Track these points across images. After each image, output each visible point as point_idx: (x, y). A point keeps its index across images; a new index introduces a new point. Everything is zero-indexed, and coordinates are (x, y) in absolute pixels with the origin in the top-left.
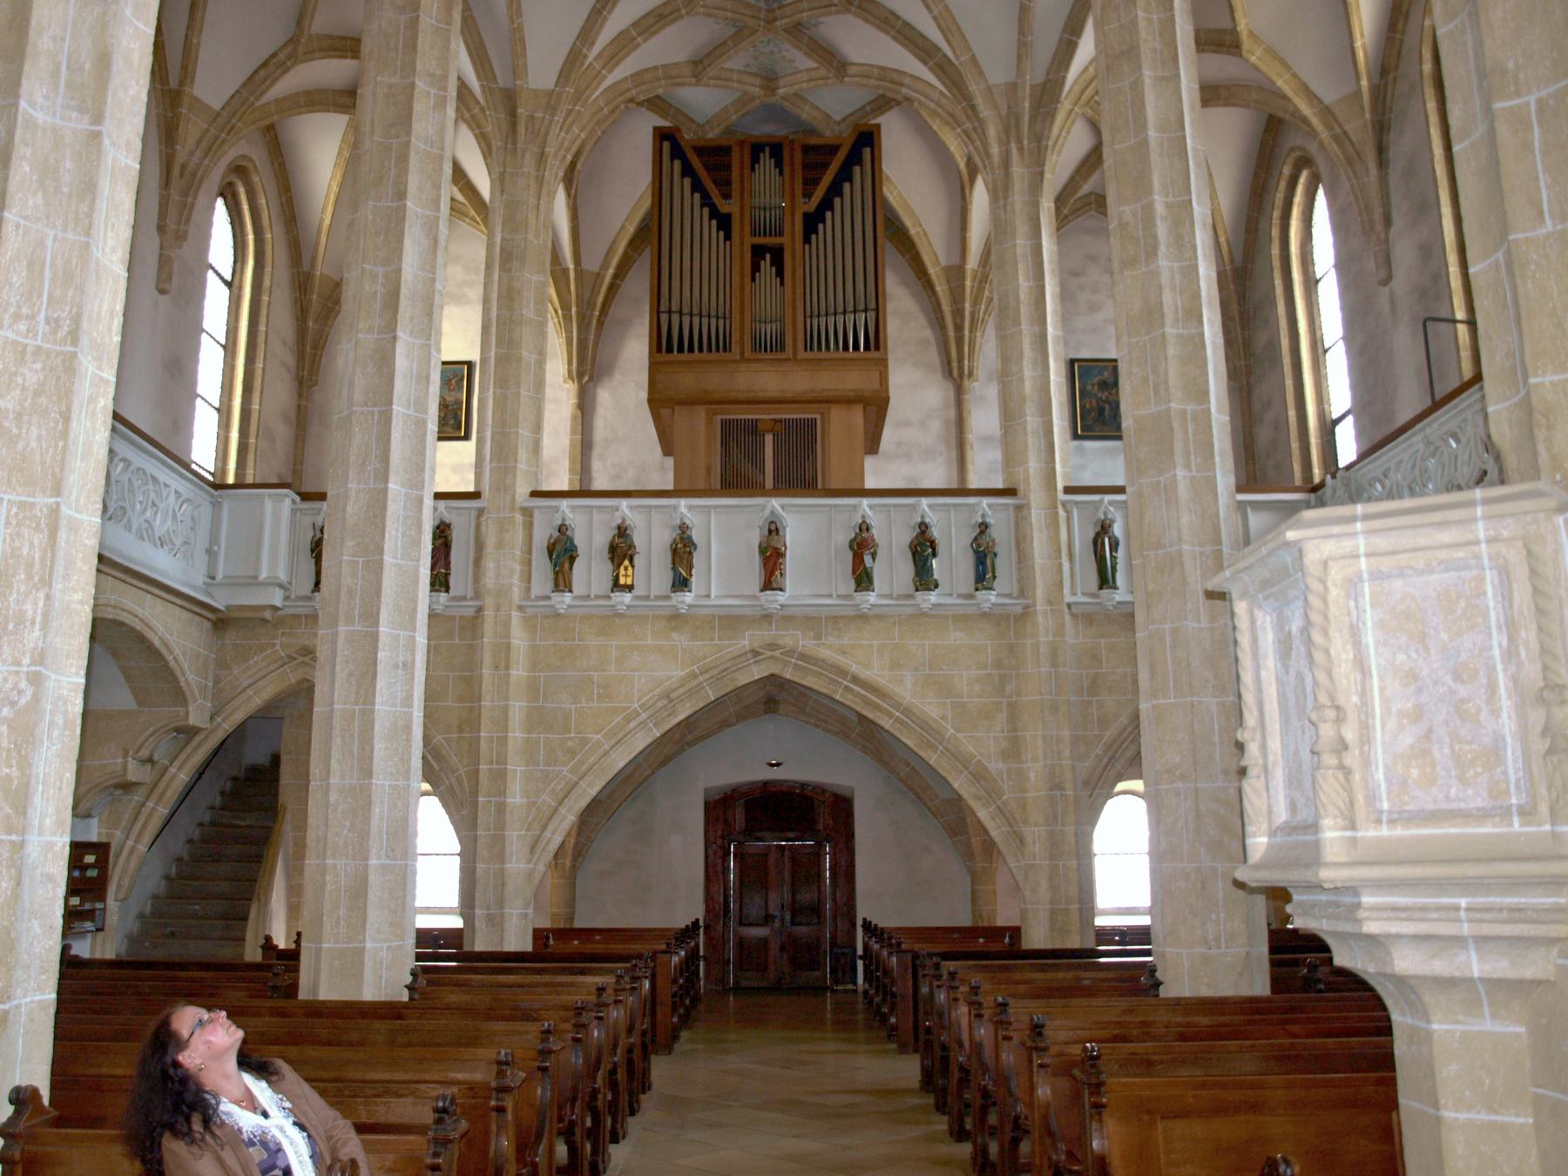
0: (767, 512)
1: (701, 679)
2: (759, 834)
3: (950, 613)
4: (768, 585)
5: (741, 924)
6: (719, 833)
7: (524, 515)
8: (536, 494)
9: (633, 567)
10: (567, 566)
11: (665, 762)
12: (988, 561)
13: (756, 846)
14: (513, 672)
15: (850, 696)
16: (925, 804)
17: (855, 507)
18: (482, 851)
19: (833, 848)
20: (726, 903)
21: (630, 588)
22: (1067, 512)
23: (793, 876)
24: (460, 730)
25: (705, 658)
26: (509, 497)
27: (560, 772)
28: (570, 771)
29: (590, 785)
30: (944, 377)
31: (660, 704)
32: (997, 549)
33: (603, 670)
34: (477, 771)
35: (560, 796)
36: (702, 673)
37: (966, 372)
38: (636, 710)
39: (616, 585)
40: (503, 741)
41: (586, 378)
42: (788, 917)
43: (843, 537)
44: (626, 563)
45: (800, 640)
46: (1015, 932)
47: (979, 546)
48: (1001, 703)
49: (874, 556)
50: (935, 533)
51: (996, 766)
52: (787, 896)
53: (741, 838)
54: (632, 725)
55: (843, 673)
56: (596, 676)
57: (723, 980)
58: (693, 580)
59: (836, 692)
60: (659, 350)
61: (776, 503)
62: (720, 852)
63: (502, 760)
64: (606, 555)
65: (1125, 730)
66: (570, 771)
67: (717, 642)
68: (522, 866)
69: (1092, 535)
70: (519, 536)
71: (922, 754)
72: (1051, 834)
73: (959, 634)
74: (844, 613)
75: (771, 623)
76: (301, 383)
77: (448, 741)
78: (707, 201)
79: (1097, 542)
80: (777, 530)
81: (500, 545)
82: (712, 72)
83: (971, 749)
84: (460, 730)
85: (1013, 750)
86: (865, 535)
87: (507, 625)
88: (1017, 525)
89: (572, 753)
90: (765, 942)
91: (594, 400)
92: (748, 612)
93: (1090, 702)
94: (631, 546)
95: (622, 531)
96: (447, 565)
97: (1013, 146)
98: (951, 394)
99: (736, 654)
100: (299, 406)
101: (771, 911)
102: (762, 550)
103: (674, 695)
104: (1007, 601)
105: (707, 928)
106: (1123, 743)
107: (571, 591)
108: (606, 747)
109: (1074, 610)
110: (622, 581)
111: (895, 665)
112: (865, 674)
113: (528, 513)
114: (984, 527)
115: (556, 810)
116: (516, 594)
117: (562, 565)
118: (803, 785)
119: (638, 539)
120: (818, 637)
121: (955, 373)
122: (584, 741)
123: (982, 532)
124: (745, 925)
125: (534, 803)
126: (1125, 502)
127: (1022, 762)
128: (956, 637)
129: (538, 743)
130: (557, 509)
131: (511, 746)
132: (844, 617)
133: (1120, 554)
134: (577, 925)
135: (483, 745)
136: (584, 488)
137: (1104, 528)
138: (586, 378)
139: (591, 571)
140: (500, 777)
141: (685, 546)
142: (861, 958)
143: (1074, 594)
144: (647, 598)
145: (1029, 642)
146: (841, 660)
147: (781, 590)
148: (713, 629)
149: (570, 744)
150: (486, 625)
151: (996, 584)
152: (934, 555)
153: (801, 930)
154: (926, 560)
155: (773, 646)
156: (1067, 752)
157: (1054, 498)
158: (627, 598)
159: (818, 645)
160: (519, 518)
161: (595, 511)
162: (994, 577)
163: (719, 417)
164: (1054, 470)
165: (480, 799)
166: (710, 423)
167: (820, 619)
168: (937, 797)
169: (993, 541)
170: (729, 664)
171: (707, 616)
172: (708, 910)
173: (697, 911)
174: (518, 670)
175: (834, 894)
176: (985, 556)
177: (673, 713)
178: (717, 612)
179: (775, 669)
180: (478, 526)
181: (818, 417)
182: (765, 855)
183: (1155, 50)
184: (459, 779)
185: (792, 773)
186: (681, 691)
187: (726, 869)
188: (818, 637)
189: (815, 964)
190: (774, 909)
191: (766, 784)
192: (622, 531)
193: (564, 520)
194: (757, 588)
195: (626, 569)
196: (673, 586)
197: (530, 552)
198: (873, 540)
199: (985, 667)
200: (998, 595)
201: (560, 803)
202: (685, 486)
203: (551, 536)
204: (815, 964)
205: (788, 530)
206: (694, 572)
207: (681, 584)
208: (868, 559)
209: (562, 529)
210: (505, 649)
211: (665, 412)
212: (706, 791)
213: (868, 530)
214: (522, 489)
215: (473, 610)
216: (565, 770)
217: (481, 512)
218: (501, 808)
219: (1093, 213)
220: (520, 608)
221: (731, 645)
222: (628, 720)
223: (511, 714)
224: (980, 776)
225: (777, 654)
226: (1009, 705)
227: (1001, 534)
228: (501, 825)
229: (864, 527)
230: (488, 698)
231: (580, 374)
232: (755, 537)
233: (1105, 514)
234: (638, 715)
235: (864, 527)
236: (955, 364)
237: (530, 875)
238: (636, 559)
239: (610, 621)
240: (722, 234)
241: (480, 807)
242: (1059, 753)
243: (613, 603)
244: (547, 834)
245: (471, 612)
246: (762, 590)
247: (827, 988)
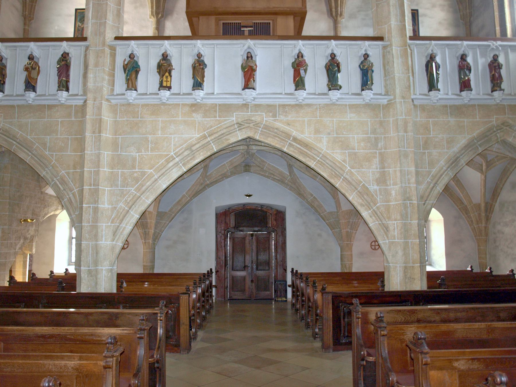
0: (246, 47)
1: (209, 139)
2: (241, 229)
3: (348, 103)
4: (247, 86)
5: (233, 270)
6: (223, 228)
7: (111, 49)
8: (117, 38)
9: (171, 76)
10: (134, 76)
11: (197, 194)
12: (369, 75)
13: (240, 234)
14: (103, 135)
15: (292, 149)
16: (319, 214)
18: (85, 234)
19: (276, 235)
20: (226, 260)
21: (169, 88)
22: (411, 50)
23: (257, 248)
24: (75, 168)
25: (211, 127)
26: (102, 38)
27: (131, 190)
28: (135, 190)
29: (147, 198)
30: (328, 17)
31: (186, 153)
32: (374, 69)
33: (154, 134)
34: (83, 190)
35: (130, 204)
36: (209, 136)
37: (339, 13)
38: (172, 156)
39: (162, 86)
40: (97, 173)
41: (160, 15)
42: (255, 267)
43: (288, 62)
44: (167, 74)
45: (266, 118)
46: (379, 276)
47: (364, 66)
48: (376, 153)
49: (305, 71)
50: (339, 59)
51: (373, 188)
52: (255, 258)
53: (233, 230)
54: (171, 164)
55: (288, 135)
57: (225, 296)
58: (205, 84)
59: (285, 147)
61: (250, 43)
62: (223, 237)
63: (97, 184)
65: (442, 168)
66: (135, 190)
67: (218, 118)
68: (108, 243)
69: (424, 63)
70: (108, 60)
71: (332, 181)
72: (405, 225)
73: (353, 115)
74: (289, 103)
75: (248, 108)
76: (25, 18)
77: (68, 173)
79: (428, 66)
80: (252, 57)
81: (96, 65)
83: (360, 178)
84: (75, 168)
85: (382, 179)
86: (300, 59)
87: (100, 108)
88: (384, 56)
89: (137, 180)
90: (244, 278)
91: (164, 27)
94: (170, 65)
95: (165, 57)
96: (68, 76)
98: (332, 24)
99: (228, 125)
100: (24, 29)
101: (246, 264)
102: (243, 68)
103: (194, 148)
105: (217, 272)
106: (441, 176)
107: (136, 90)
108: (156, 177)
110: (165, 84)
111: (317, 131)
112: (300, 136)
113: (113, 49)
114: (366, 56)
116: (106, 91)
117: (131, 76)
118: (262, 206)
119: (174, 63)
120: (274, 116)
121: (334, 14)
122: (144, 173)
123: (365, 59)
124: (235, 270)
125: (115, 208)
127: (387, 185)
128: (351, 116)
129: (118, 174)
131: (101, 175)
132: (289, 105)
133: (440, 72)
134: (156, 271)
135: (86, 174)
137: (432, 58)
138: (160, 15)
140: (95, 193)
141: (200, 65)
142: (289, 286)
145: (391, 119)
146: (287, 128)
147: (254, 89)
148: (215, 111)
149: (135, 175)
150: (88, 109)
151: (373, 87)
152: (339, 71)
153: (260, 273)
154: (335, 74)
155: (249, 121)
156: (413, 180)
157: (406, 42)
158: (167, 93)
159: (275, 120)
160: (107, 50)
162: (372, 84)
163: (222, 22)
164: (405, 26)
165: (84, 205)
166: (217, 24)
168: (326, 211)
169: (372, 64)
170: (225, 131)
171: (213, 104)
172: (218, 263)
173: (212, 265)
174: (106, 134)
175: (276, 256)
176: (367, 72)
177: (193, 158)
179: (250, 134)
180: (86, 56)
181: (271, 22)
182: (244, 239)
184: (74, 195)
185: (256, 200)
186: (197, 146)
187: (225, 246)
188: (274, 116)
189: (267, 288)
190: (248, 263)
191: (244, 205)
192: (165, 57)
193: (132, 51)
194: (241, 89)
195: (167, 77)
196: (193, 87)
197: (114, 70)
198: (305, 62)
199: (367, 134)
200: (374, 94)
203: (125, 60)
204: (267, 288)
205: (257, 57)
206: (205, 79)
207: (198, 85)
208: (302, 72)
209: (132, 56)
210: (99, 123)
211: (195, 20)
212: (216, 208)
213: (302, 57)
214: (110, 35)
215: (83, 101)
216: (133, 190)
217: (87, 48)
218: (96, 210)
220: (108, 100)
221: (225, 120)
223: (101, 158)
224: (364, 193)
225: (251, 125)
226: (380, 154)
227: (375, 59)
228: (96, 220)
229: (300, 55)
230: (89, 149)
231: (157, 14)
232: (239, 61)
233: (432, 51)
235: (300, 55)
236: (334, 10)
237: (113, 248)
238: (173, 73)
241: (84, 210)
242: (409, 180)
244: (123, 225)
245: (81, 103)
246: (243, 90)
247: (273, 299)
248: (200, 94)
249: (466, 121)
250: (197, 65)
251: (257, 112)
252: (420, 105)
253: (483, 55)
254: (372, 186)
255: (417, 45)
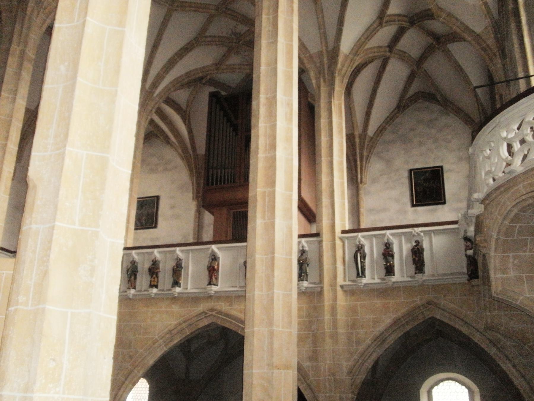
0: (210, 251)
17: (356, 237)
27: (127, 365)
44: (155, 276)
45: (223, 306)
56: (142, 324)
60: (208, 184)
64: (171, 272)
78: (229, 120)
82: (223, 67)
92: (202, 295)
93: (352, 333)
97: (322, 80)
102: (208, 268)
103: (173, 332)
104: (314, 286)
109: (345, 289)
115: (124, 382)
120: (231, 305)
122: (137, 352)
126: (458, 228)
130: (130, 254)
136: (200, 241)
139: (143, 280)
143: (345, 281)
144: (140, 291)
155: (212, 310)
161: (146, 255)
167: (232, 297)
178: (192, 296)
183: (269, 31)
186: (176, 330)
188: (231, 305)
201: (126, 379)
202: (217, 239)
219: (421, 101)
222: (154, 343)
227: (312, 256)
232: (206, 262)
234: (158, 341)
239: (149, 300)
240: (234, 132)
243: (148, 293)
248: (178, 290)
249: (391, 302)
250: (175, 267)
251: (218, 302)
252: (349, 291)
253: (408, 241)
254: (305, 363)
255: (347, 238)
